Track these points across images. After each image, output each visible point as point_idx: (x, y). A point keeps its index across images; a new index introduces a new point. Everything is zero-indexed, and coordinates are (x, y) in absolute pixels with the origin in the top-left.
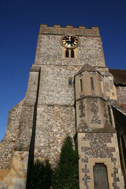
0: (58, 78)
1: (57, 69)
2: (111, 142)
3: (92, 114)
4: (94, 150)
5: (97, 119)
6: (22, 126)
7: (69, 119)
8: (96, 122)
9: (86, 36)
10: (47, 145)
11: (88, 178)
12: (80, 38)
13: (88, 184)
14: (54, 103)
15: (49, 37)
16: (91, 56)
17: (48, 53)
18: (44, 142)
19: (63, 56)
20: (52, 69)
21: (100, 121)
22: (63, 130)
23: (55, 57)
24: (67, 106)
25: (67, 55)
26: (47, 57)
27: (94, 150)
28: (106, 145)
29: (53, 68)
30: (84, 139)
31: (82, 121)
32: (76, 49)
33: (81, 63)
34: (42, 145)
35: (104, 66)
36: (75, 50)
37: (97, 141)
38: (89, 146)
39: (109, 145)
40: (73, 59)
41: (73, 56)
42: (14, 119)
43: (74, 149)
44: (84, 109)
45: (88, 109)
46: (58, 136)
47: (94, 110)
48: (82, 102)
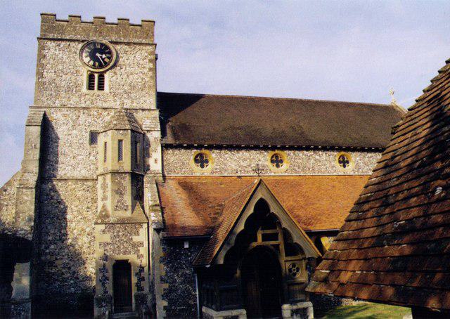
0: (74, 132)
1: (72, 114)
2: (138, 235)
3: (117, 197)
4: (116, 246)
5: (123, 204)
6: (30, 154)
7: (89, 200)
8: (121, 208)
9: (128, 44)
10: (58, 238)
11: (107, 279)
12: (118, 47)
13: (106, 285)
14: (68, 175)
15: (59, 45)
16: (133, 88)
17: (58, 81)
18: (54, 234)
19: (84, 89)
20: (65, 115)
21: (127, 206)
22: (80, 217)
23: (69, 90)
24: (86, 180)
25: (91, 87)
26: (55, 92)
27: (116, 246)
28: (132, 239)
29: (67, 113)
30: (104, 231)
31: (104, 206)
32: (108, 73)
33: (115, 101)
34: (50, 238)
35: (155, 108)
36: (107, 76)
37: (120, 234)
38: (109, 241)
39: (136, 239)
40: (100, 92)
41: (101, 87)
42: (5, 203)
43: (445, 172)
44: (107, 189)
45: (112, 190)
46: (74, 224)
47: (119, 191)
48: (104, 179)
